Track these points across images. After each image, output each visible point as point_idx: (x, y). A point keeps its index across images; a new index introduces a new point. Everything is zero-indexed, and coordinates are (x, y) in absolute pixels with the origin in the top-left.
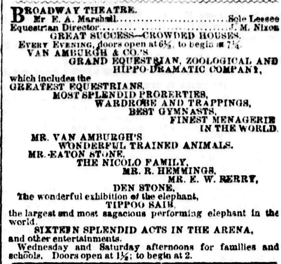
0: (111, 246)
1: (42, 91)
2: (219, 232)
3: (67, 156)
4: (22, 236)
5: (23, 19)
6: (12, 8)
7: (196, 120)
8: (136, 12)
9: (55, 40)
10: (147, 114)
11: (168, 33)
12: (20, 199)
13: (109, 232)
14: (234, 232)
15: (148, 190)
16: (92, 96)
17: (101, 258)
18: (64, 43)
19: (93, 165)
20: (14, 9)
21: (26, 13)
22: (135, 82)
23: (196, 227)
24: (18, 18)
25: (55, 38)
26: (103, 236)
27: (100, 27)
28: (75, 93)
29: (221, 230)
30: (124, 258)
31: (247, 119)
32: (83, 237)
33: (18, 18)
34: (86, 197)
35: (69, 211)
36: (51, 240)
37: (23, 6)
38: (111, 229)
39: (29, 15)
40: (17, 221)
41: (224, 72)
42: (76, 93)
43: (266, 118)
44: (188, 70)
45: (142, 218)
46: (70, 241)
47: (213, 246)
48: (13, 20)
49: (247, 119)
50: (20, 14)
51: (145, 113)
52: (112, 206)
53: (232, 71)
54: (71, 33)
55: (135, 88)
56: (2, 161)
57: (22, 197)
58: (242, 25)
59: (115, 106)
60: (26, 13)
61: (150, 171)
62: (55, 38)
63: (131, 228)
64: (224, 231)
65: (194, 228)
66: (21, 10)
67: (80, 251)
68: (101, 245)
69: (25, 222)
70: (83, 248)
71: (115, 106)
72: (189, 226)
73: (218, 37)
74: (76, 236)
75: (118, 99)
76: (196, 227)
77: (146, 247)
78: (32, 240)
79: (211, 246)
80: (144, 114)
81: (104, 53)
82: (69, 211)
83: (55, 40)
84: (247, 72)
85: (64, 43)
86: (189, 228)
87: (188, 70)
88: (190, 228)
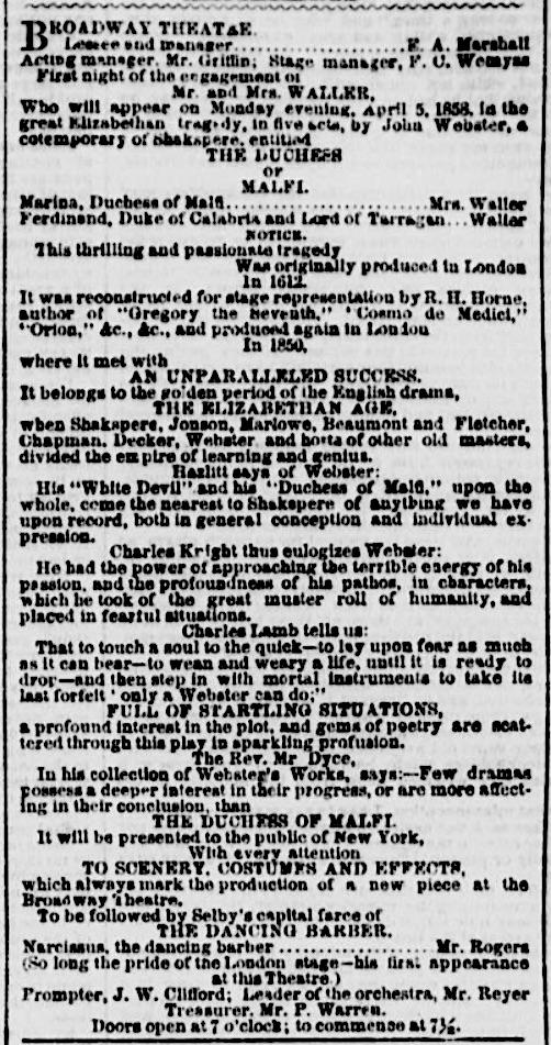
0: (156, 897)
5: (44, 43)
6: (23, 23)
8: (390, 936)
12: (41, 254)
15: (259, 872)
17: (184, 1030)
18: (240, 381)
20: (29, 24)
21: (52, 32)
30: (446, 1031)
33: (37, 42)
34: (356, 219)
35: (170, 246)
39: (56, 36)
48: (25, 45)
50: (39, 34)
52: (168, 932)
55: (161, 872)
57: (46, 250)
60: (52, 32)
66: (42, 26)
67: (333, 1022)
69: (464, 996)
70: (280, 442)
73: (127, 714)
75: (207, 941)
82: (170, 246)
85: (240, 381)
86: (153, 713)
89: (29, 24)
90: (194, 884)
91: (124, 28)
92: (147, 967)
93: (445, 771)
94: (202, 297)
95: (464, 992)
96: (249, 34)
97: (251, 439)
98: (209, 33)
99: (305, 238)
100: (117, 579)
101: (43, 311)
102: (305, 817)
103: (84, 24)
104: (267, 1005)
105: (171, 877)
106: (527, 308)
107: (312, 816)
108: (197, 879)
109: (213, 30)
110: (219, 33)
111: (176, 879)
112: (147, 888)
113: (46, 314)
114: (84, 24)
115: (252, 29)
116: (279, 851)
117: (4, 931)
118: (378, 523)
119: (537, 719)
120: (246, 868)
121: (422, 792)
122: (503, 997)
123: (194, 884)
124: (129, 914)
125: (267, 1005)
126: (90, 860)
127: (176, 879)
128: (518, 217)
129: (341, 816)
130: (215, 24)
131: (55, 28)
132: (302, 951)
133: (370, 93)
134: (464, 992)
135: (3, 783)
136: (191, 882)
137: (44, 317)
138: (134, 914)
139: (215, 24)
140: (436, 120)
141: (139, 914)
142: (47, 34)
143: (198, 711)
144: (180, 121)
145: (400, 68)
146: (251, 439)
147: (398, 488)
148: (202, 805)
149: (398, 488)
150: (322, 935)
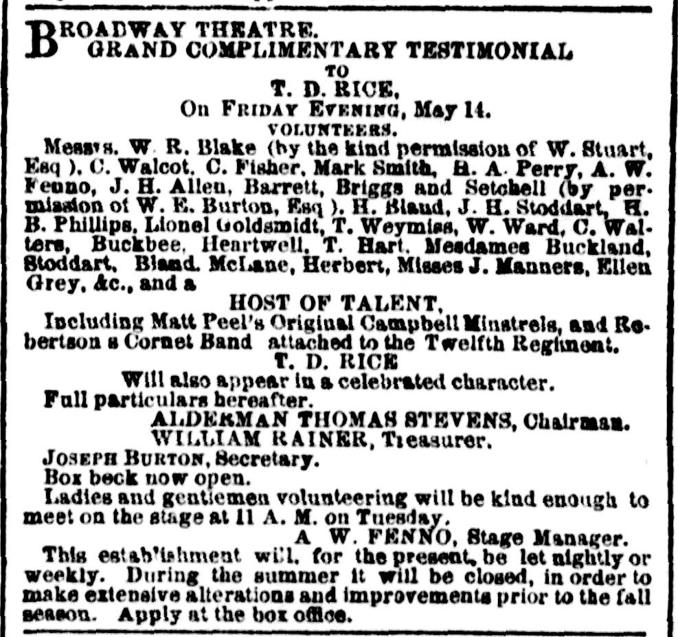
1: (388, 59)
6: (28, 23)
7: (436, 49)
10: (448, 55)
13: (313, 53)
14: (309, 56)
16: (245, 52)
19: (300, 56)
20: (35, 25)
22: (515, 61)
24: (44, 46)
26: (232, 317)
32: (150, 591)
36: (190, 480)
37: (55, 17)
38: (316, 47)
40: (512, 52)
41: (221, 55)
43: (470, 45)
46: (301, 192)
47: (649, 556)
48: (30, 50)
51: (444, 54)
53: (241, 55)
59: (367, 56)
60: (63, 35)
61: (119, 49)
63: (262, 106)
68: (375, 163)
71: (367, 56)
74: (130, 394)
77: (414, 189)
78: (242, 229)
79: (644, 556)
80: (440, 57)
81: (45, 37)
84: (145, 55)
89: (35, 25)
90: (221, 614)
91: (151, 30)
92: (523, 601)
93: (596, 428)
94: (319, 556)
95: (545, 381)
99: (350, 620)
100: (328, 589)
102: (312, 299)
103: (102, 26)
104: (303, 511)
105: (351, 160)
107: (320, 298)
108: (225, 608)
111: (356, 162)
112: (274, 574)
114: (102, 26)
116: (121, 619)
117: (305, 5)
119: (656, 319)
120: (525, 208)
121: (502, 561)
122: (68, 287)
123: (221, 614)
125: (303, 511)
127: (356, 162)
128: (167, 260)
129: (362, 414)
131: (66, 28)
133: (114, 148)
134: (545, 381)
135: (132, 4)
136: (217, 611)
140: (140, 199)
142: (56, 37)
145: (84, 289)
147: (512, 267)
148: (223, 185)
149: (512, 267)
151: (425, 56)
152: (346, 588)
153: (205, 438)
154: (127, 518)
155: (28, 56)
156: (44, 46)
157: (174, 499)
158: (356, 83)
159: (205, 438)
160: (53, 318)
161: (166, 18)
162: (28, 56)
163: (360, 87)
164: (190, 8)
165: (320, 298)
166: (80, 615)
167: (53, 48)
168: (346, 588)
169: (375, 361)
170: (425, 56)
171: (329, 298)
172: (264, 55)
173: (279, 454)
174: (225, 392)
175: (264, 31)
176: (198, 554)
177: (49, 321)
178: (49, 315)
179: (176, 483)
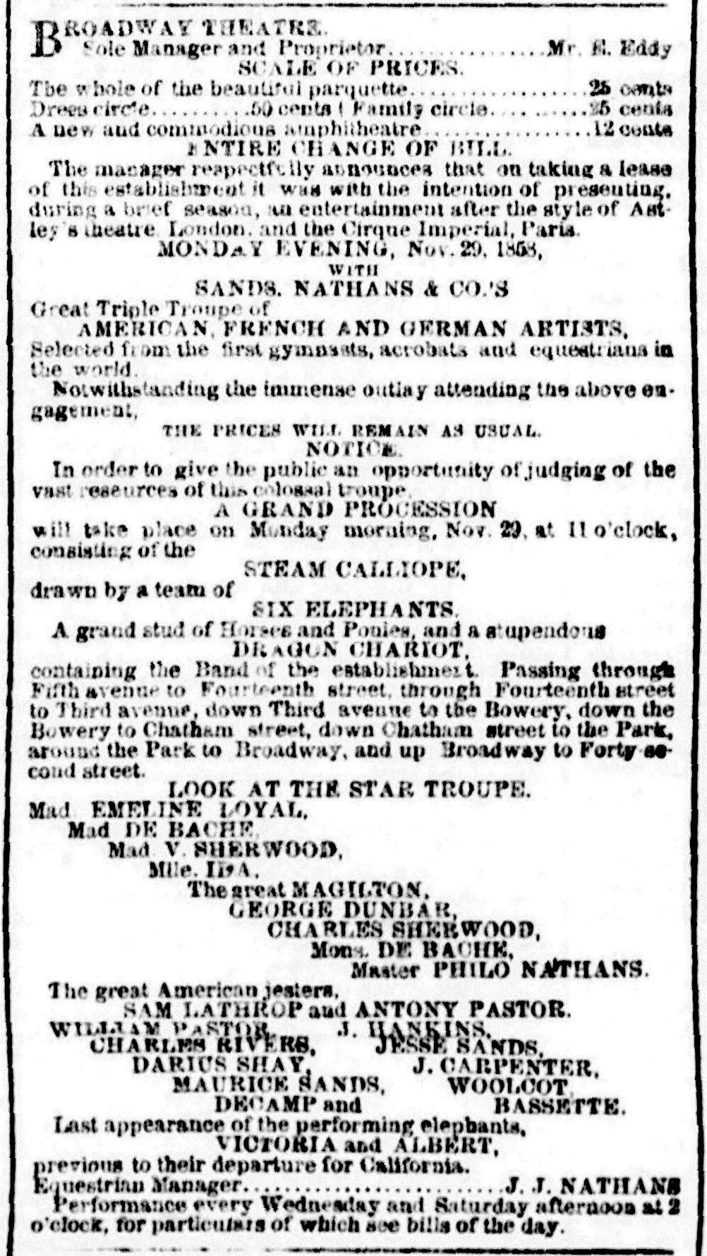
2: (162, 1070)
3: (337, 293)
4: (137, 1134)
9: (254, 519)
11: (337, 266)
23: (616, 1180)
25: (255, 513)
27: (192, 708)
28: (334, 285)
29: (396, 791)
31: (373, 146)
42: (337, 283)
44: (330, 290)
45: (664, 139)
48: (34, 51)
49: (373, 146)
54: (155, 823)
56: (14, 1066)
58: (254, 524)
62: (255, 513)
64: (583, 1072)
65: (613, 1183)
72: (101, 299)
76: (577, 963)
83: (254, 519)
86: (273, 706)
87: (330, 290)
88: (431, 784)
96: (616, 1112)
97: (553, 1226)
98: (590, 1192)
101: (593, 687)
106: (30, 369)
107: (427, 143)
109: (596, 1187)
110: (603, 1190)
113: (597, 691)
115: (620, 1107)
118: (363, 755)
124: (607, 708)
126: (434, 599)
130: (268, 783)
132: (393, 1191)
137: (593, 695)
138: (613, 707)
139: (268, 783)
141: (619, 708)
142: (60, 36)
143: (543, 211)
144: (32, 708)
146: (553, 1226)
150: (371, 976)
151: (607, 1112)
152: (622, 162)
153: (389, 569)
154: (196, 732)
155: (33, 55)
156: (48, 46)
157: (68, 413)
158: (408, 63)
159: (389, 569)
160: (61, 468)
161: (173, 16)
162: (33, 55)
163: (412, 66)
164: (298, 5)
165: (427, 143)
166: (512, 170)
167: (58, 47)
168: (622, 162)
169: (266, 1084)
170: (607, 1112)
171: (357, 755)
172: (382, 574)
173: (361, 664)
174: (359, 140)
175: (272, 28)
176: (224, 729)
177: (57, 470)
178: (56, 464)
179: (609, 715)
